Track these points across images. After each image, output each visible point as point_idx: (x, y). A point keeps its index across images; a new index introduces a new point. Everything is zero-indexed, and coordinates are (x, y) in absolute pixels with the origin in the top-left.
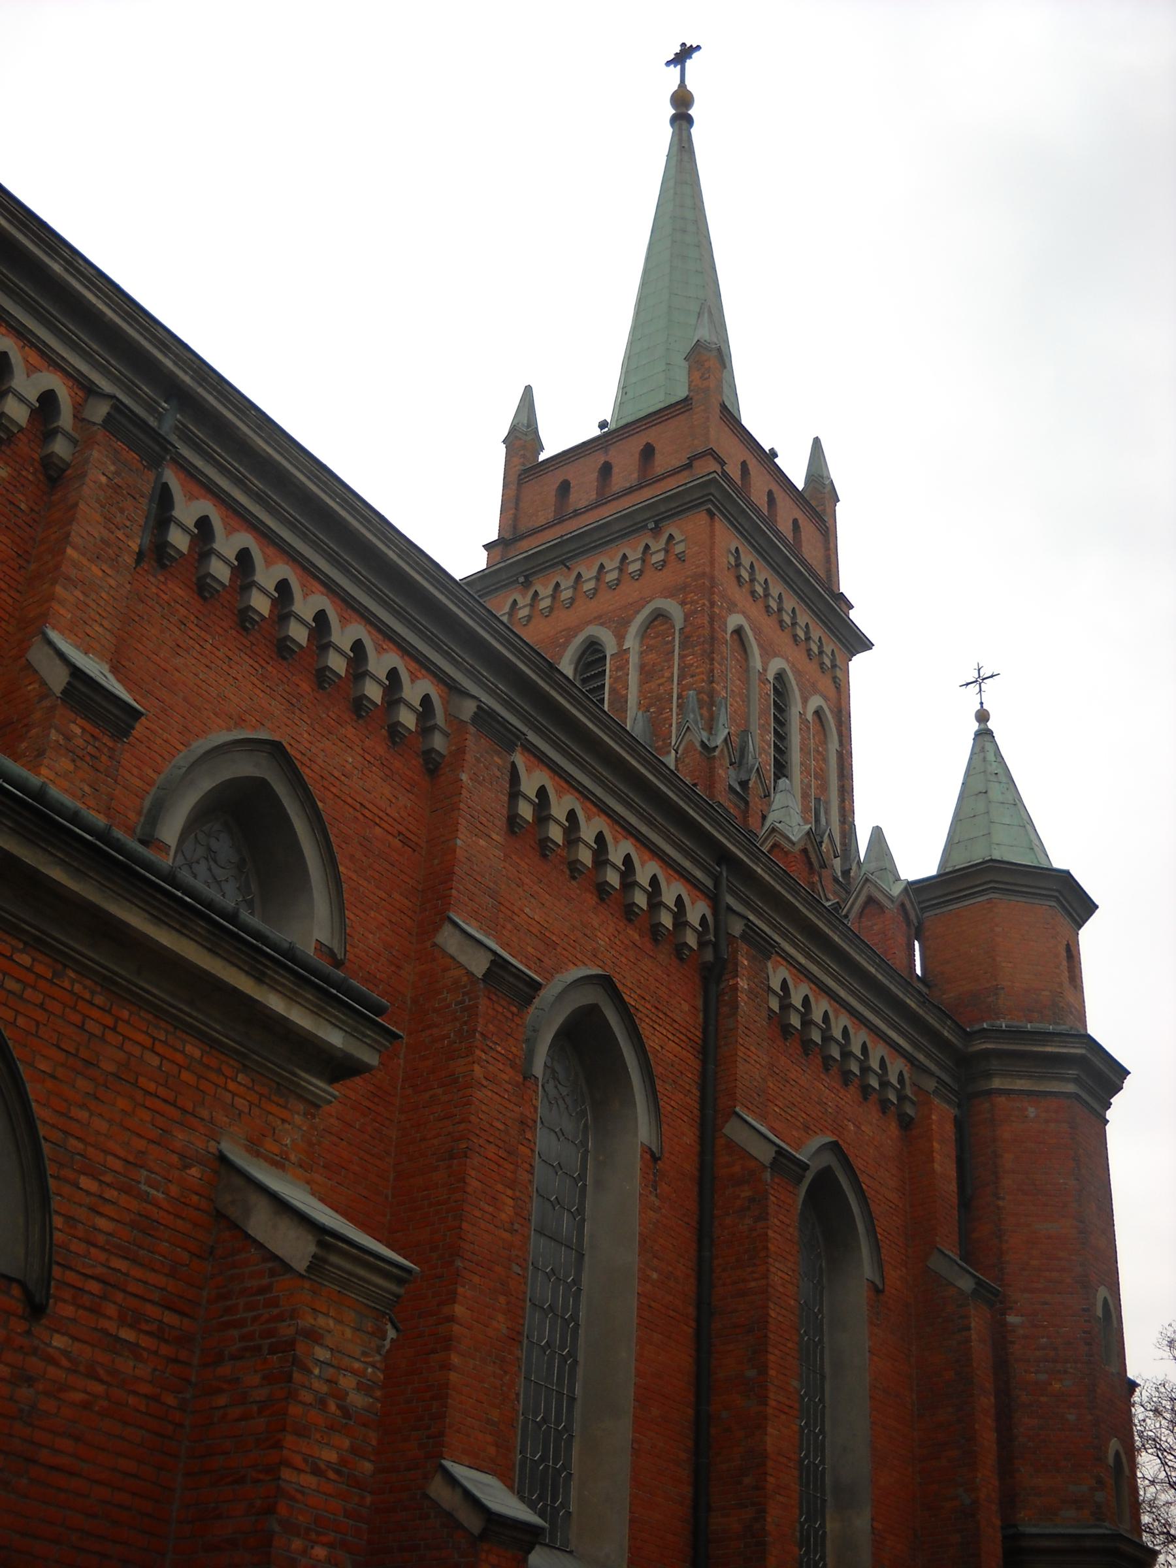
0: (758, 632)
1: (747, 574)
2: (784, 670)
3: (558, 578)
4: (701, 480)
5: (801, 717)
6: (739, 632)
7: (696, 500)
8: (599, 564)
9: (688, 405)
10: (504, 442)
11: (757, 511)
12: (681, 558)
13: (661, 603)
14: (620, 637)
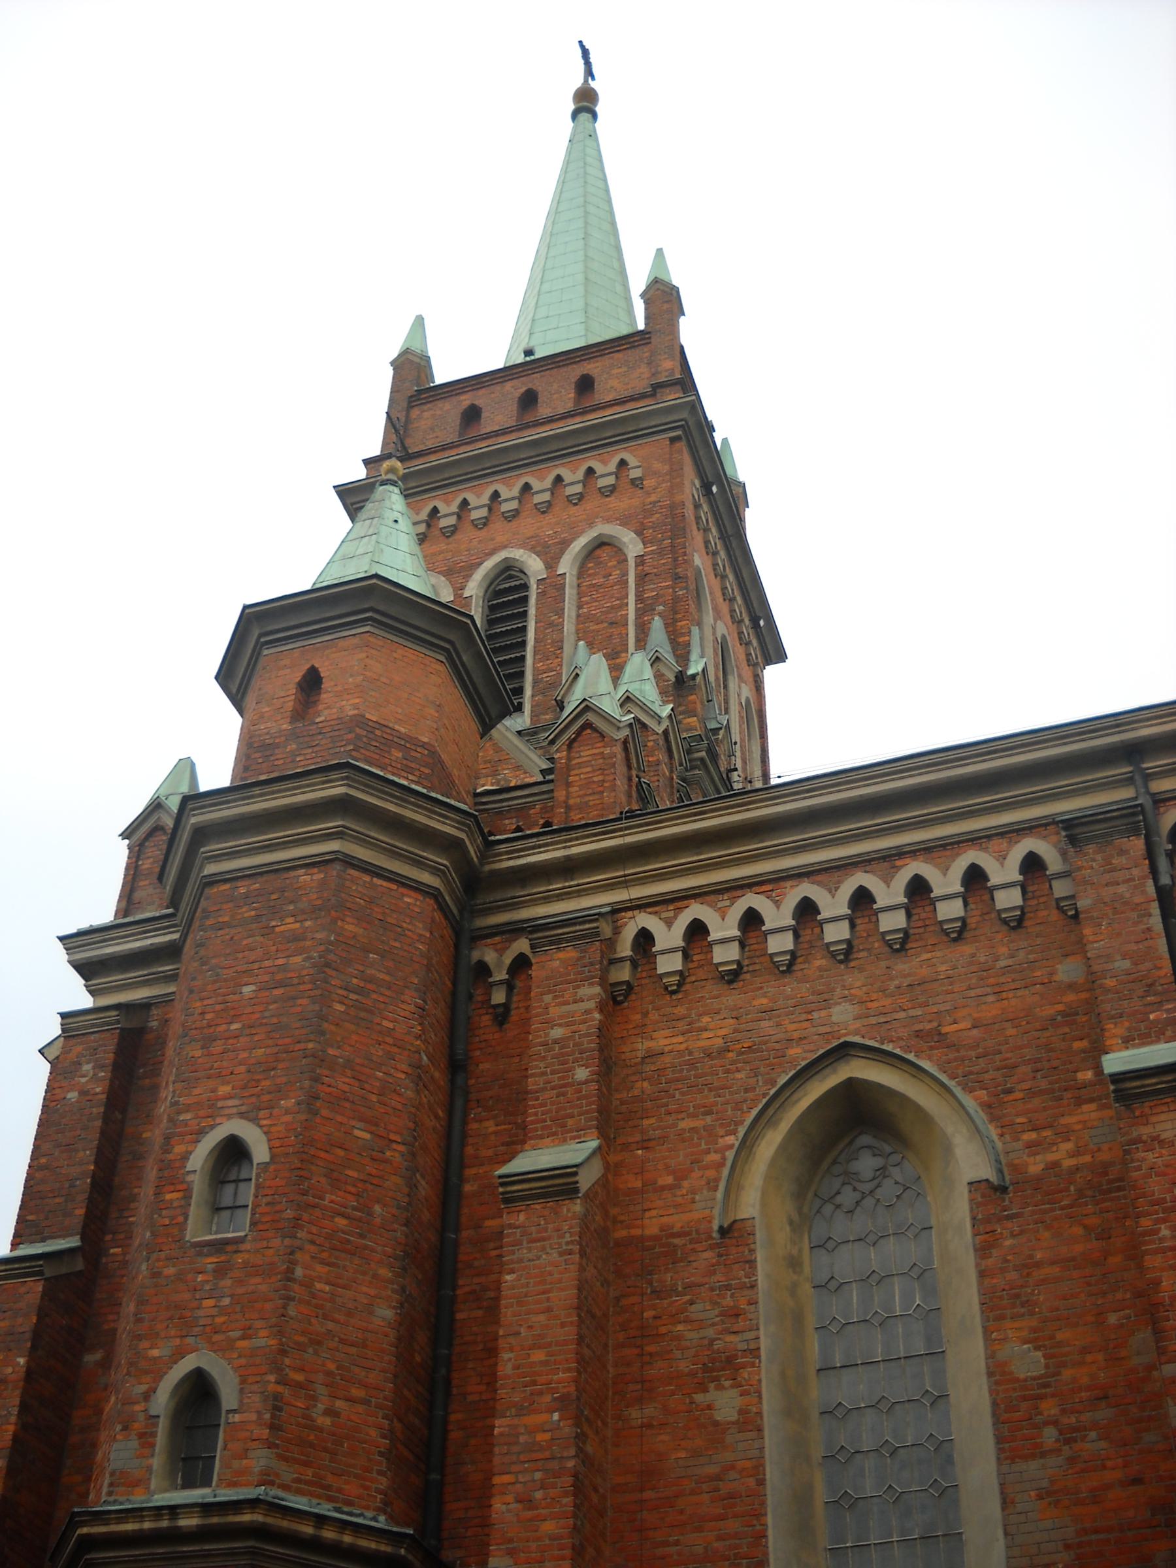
3: (562, 471)
4: (480, 451)
7: (629, 433)
8: (432, 506)
9: (645, 339)
10: (392, 363)
12: (636, 483)
13: (517, 554)
14: (551, 564)
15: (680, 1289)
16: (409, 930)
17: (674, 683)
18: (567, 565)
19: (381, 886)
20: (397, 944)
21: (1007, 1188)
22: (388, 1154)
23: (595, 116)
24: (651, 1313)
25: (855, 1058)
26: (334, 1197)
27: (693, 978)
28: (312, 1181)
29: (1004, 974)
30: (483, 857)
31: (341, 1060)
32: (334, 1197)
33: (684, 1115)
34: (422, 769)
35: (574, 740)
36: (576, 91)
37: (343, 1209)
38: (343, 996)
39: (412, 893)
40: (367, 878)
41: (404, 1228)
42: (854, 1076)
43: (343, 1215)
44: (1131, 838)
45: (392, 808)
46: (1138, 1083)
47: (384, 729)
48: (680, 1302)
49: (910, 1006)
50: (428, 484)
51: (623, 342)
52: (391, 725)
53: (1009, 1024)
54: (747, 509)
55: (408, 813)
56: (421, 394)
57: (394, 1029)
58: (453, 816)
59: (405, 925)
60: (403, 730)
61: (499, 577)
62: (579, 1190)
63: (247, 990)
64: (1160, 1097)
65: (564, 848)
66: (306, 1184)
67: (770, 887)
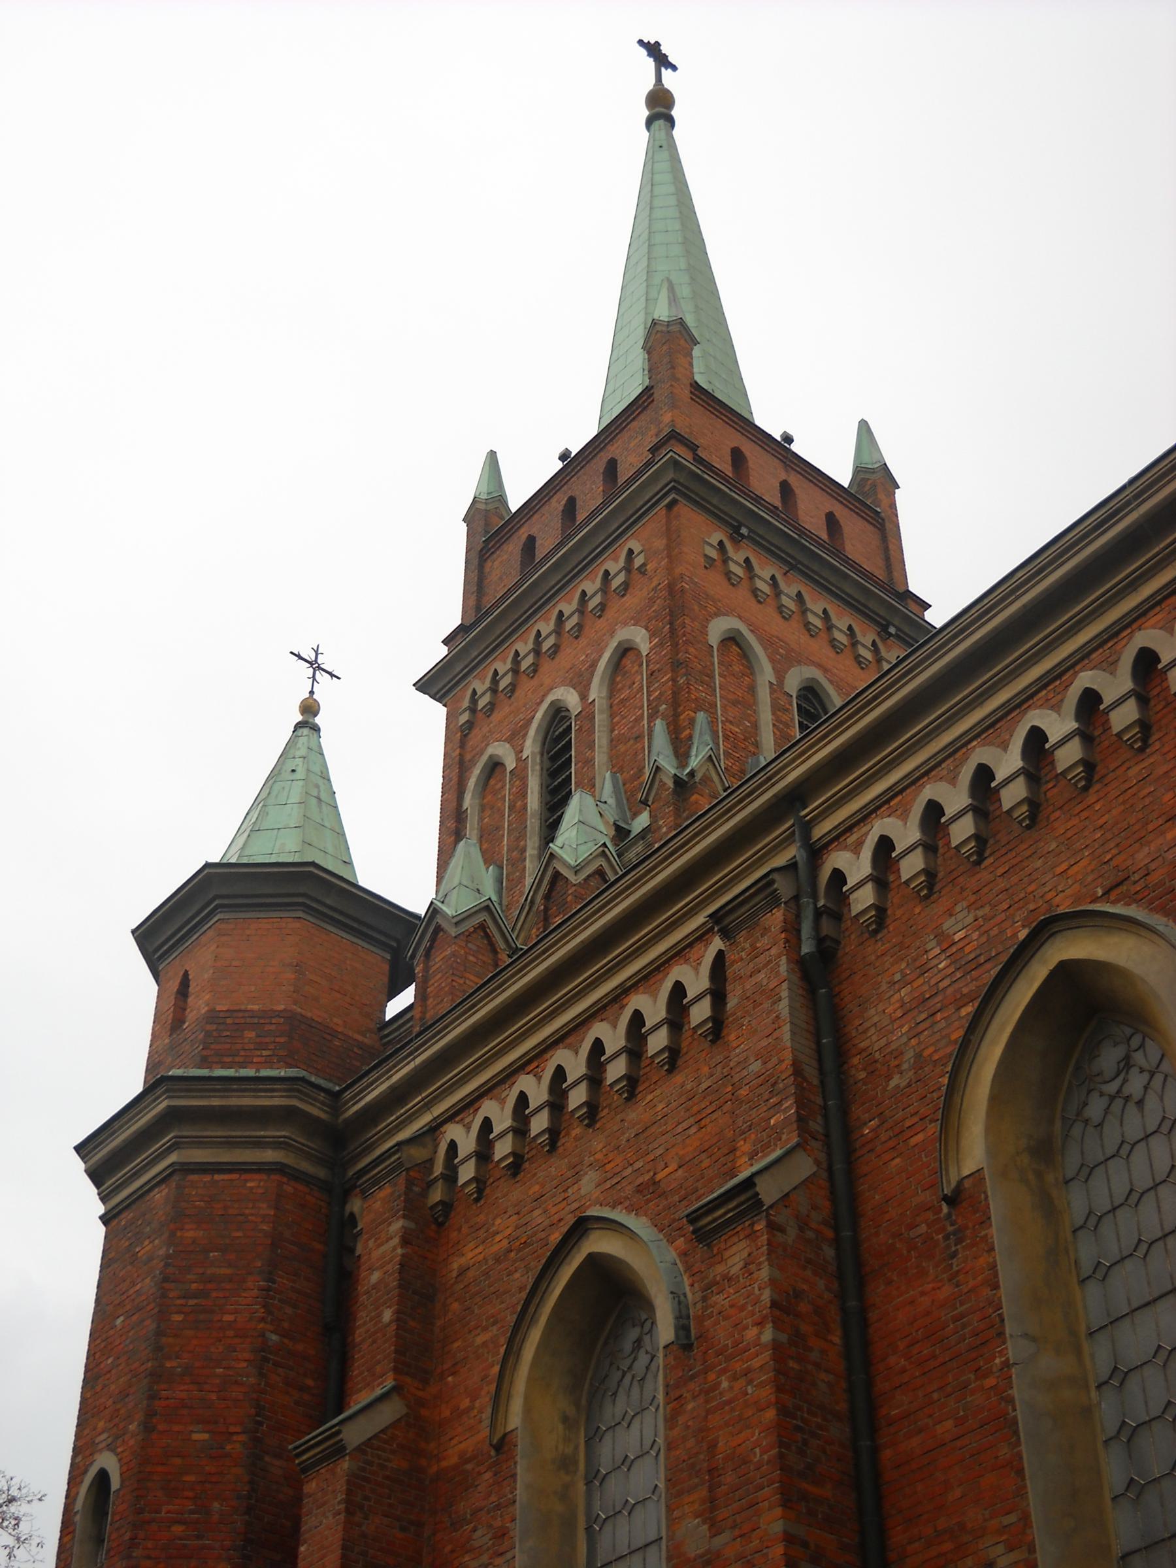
0: (768, 643)
1: (845, 637)
2: (738, 631)
5: (770, 687)
6: (732, 640)
10: (464, 520)
11: (724, 478)
12: (642, 570)
15: (469, 1516)
16: (252, 1215)
17: (675, 791)
18: (597, 692)
19: (223, 1180)
20: (239, 1234)
21: (693, 1344)
22: (228, 1447)
23: (671, 121)
24: (449, 1548)
25: (594, 1231)
26: (170, 1507)
27: (491, 1180)
28: (149, 1498)
29: (705, 1098)
30: (336, 1110)
31: (179, 1370)
32: (170, 1507)
33: (479, 1330)
34: (277, 1040)
35: (431, 946)
36: (646, 98)
37: (180, 1516)
38: (182, 1305)
39: (256, 1176)
40: (207, 1178)
41: (247, 1517)
42: (591, 1251)
43: (179, 1522)
44: (773, 912)
45: (216, 1102)
46: (709, 1218)
47: (235, 1014)
48: (468, 1530)
49: (635, 1159)
50: (487, 648)
51: (635, 408)
52: (243, 1007)
53: (704, 1156)
54: (897, 491)
55: (234, 1102)
56: (488, 544)
57: (235, 1320)
58: (279, 1087)
59: (247, 1211)
60: (256, 1007)
61: (552, 724)
62: (345, 1447)
63: (119, 1321)
64: (733, 1227)
65: (388, 1079)
66: (142, 1503)
67: (535, 1064)
